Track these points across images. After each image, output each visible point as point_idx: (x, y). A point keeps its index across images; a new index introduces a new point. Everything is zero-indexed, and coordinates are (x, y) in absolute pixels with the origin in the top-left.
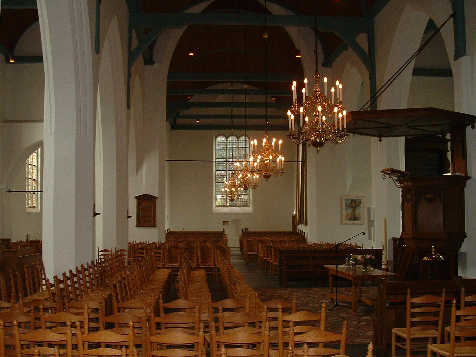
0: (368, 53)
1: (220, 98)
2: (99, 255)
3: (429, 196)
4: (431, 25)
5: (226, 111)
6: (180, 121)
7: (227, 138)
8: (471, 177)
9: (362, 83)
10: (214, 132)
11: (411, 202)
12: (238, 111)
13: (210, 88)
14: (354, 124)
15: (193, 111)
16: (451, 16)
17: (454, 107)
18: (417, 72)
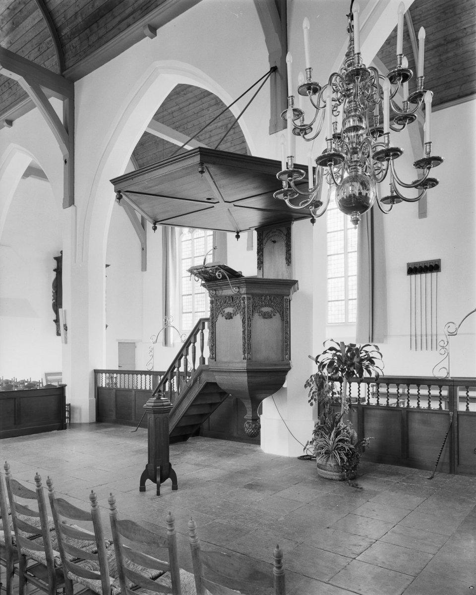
3: (265, 309)
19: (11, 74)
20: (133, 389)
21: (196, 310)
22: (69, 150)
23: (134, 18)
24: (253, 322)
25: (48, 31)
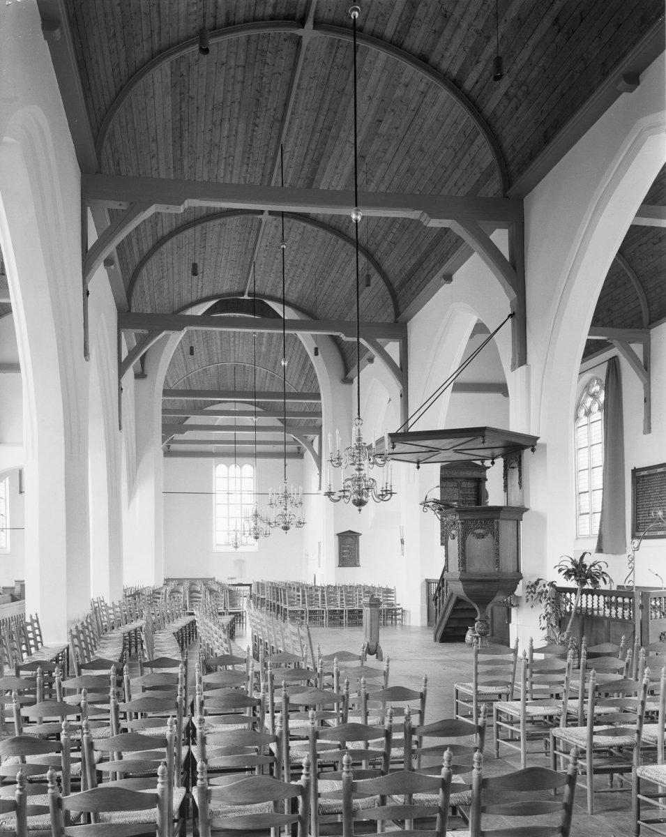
0: (399, 366)
1: (220, 420)
2: (513, 674)
3: (478, 531)
4: (480, 328)
5: (229, 435)
6: (174, 447)
7: (228, 467)
8: (527, 510)
9: (390, 400)
10: (213, 460)
11: (457, 538)
12: (242, 435)
13: (208, 408)
14: (393, 448)
15: (189, 435)
16: (511, 316)
17: (509, 427)
18: (454, 390)
19: (440, 223)
20: (604, 617)
21: (593, 511)
22: (403, 385)
23: (436, 270)
24: (467, 542)
25: (385, 287)
